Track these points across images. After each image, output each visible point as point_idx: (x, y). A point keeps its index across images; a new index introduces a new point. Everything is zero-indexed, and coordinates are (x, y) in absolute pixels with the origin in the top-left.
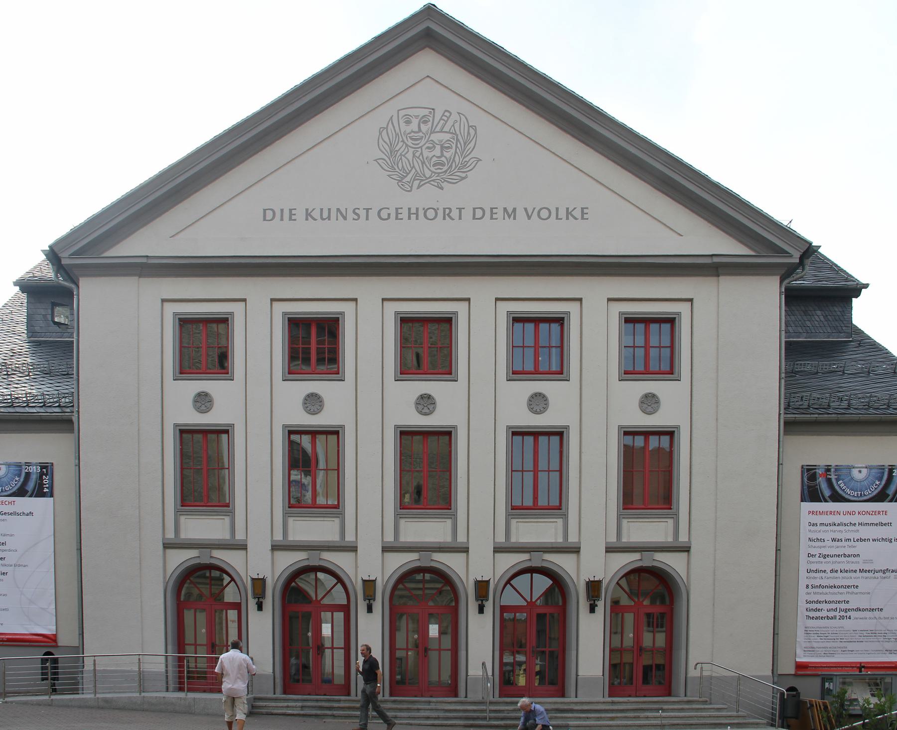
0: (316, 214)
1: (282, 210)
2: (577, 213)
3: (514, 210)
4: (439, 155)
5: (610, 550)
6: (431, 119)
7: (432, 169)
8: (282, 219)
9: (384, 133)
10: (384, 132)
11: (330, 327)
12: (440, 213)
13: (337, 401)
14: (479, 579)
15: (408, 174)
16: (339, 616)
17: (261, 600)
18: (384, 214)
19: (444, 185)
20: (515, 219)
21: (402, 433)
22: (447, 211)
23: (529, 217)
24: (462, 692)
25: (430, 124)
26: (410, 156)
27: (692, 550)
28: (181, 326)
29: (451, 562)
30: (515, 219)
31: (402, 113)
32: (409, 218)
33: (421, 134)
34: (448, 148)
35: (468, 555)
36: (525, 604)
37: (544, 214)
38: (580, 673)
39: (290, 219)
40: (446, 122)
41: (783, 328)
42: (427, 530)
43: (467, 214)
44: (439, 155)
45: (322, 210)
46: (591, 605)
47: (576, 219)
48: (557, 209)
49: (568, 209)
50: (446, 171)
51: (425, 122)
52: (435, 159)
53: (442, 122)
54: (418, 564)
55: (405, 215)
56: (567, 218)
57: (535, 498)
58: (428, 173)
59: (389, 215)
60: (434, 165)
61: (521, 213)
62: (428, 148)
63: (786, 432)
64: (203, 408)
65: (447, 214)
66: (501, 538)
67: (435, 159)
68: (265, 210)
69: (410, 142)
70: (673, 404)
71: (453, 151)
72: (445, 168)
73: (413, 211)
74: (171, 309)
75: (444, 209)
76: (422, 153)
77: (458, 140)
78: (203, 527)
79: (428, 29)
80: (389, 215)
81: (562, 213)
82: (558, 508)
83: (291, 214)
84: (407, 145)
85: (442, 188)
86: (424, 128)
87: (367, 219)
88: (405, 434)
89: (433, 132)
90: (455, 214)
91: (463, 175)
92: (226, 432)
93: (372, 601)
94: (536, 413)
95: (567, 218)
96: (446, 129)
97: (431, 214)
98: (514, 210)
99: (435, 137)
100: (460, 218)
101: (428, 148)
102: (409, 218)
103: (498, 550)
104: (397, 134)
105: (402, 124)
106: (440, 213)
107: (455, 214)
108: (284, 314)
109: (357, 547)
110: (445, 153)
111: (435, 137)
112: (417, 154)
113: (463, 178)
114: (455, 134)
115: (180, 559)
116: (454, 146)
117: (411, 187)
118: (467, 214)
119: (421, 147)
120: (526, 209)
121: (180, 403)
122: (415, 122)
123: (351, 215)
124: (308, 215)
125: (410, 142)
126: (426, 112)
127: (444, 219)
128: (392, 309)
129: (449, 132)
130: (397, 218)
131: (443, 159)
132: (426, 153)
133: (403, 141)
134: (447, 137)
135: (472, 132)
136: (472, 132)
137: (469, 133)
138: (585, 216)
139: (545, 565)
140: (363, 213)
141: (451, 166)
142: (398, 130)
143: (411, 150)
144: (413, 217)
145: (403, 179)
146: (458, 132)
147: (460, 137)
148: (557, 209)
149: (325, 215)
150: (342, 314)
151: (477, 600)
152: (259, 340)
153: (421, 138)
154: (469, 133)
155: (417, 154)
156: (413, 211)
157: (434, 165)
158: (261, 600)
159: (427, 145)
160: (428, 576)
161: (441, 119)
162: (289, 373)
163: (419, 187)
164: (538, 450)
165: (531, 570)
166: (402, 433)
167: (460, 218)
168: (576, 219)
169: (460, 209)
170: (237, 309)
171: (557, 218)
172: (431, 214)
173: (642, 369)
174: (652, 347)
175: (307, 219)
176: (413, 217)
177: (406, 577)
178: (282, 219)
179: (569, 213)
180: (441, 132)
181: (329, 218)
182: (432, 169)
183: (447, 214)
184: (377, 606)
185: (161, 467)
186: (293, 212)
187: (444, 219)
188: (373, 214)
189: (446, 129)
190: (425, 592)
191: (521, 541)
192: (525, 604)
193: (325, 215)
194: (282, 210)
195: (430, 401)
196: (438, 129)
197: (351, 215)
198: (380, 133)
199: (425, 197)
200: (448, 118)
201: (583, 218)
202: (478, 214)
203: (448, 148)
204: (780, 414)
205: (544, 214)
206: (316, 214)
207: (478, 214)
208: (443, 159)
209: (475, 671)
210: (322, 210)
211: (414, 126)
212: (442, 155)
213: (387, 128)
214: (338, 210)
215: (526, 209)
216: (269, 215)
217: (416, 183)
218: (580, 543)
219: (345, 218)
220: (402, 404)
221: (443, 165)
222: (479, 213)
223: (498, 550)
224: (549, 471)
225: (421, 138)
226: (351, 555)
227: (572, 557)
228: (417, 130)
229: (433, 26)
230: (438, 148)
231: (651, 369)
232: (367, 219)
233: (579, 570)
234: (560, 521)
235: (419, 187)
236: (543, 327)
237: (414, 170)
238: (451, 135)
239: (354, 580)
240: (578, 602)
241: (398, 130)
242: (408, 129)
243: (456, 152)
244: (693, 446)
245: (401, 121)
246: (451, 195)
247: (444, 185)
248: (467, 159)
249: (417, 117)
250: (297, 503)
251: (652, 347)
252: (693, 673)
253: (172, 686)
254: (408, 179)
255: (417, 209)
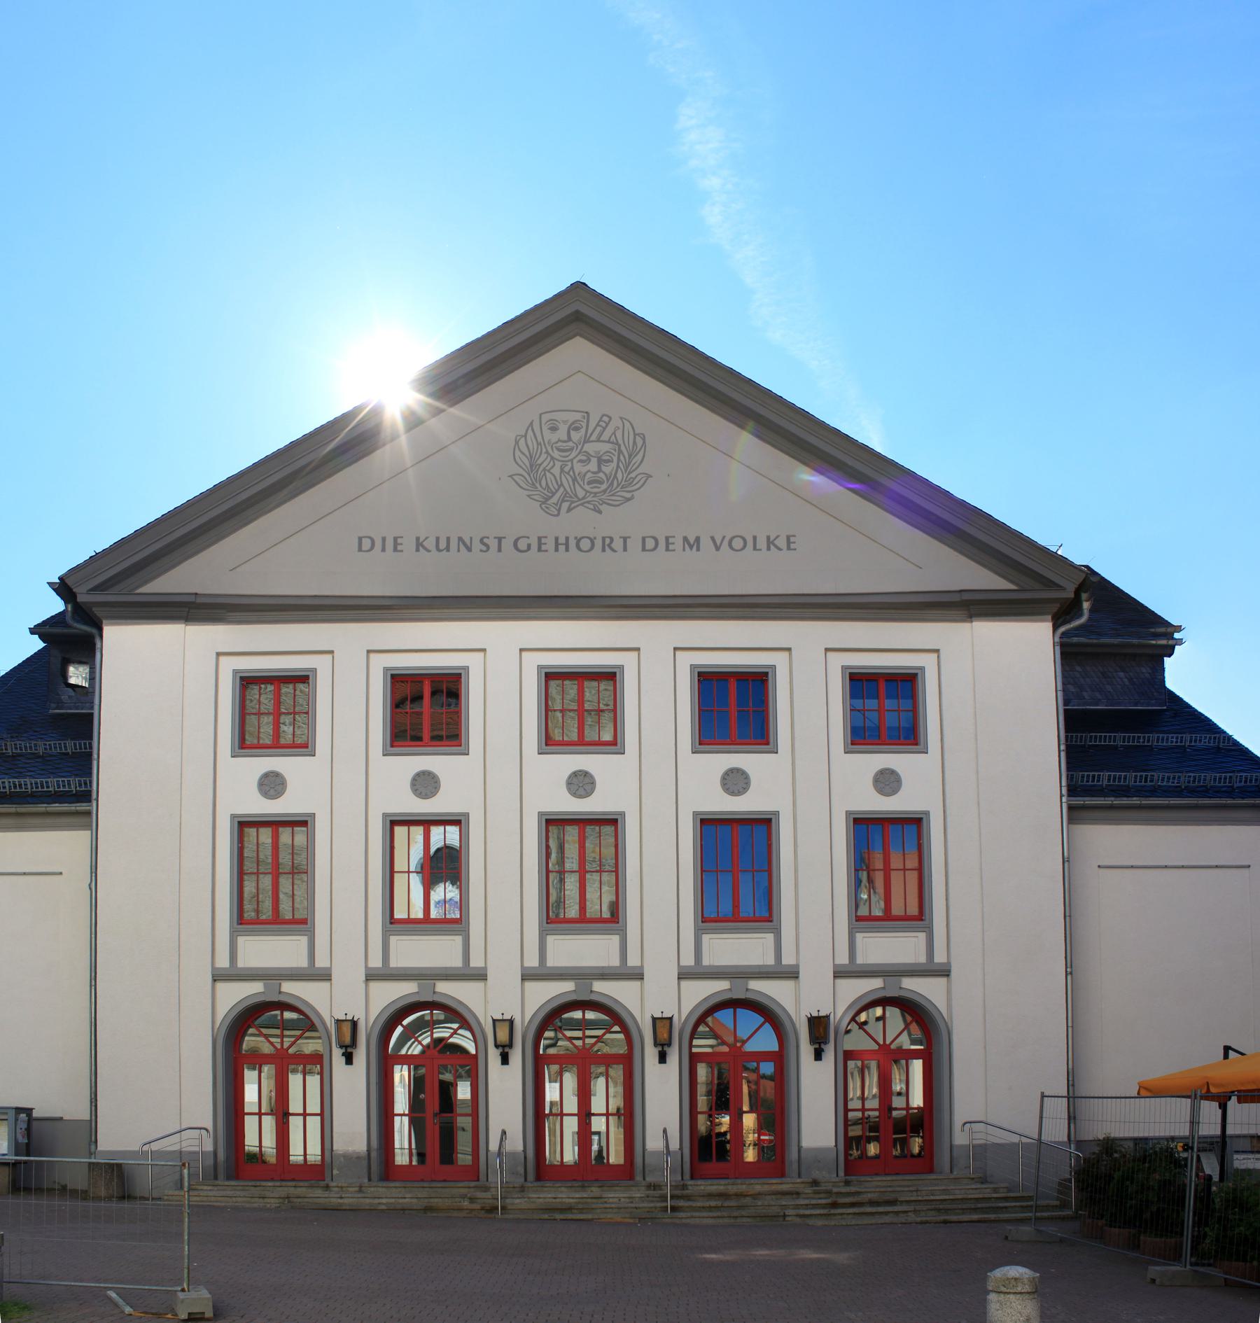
0: (430, 544)
1: (384, 539)
2: (782, 542)
3: (698, 540)
4: (595, 469)
5: (528, 976)
6: (584, 425)
7: (587, 487)
8: (383, 550)
9: (522, 442)
10: (522, 442)
11: (754, 686)
12: (598, 543)
13: (769, 781)
14: (815, 1014)
15: (554, 494)
16: (617, 1072)
17: (666, 1048)
18: (522, 545)
19: (603, 507)
20: (698, 550)
21: (703, 822)
22: (608, 541)
23: (718, 548)
24: (482, 1177)
25: (583, 431)
26: (556, 471)
27: (953, 974)
28: (393, 684)
29: (775, 991)
30: (698, 550)
31: (545, 418)
32: (557, 550)
33: (570, 444)
34: (608, 461)
35: (949, 982)
36: (877, 1047)
37: (738, 543)
38: (335, 1148)
39: (395, 550)
40: (604, 429)
41: (1060, 687)
42: (739, 949)
43: (634, 545)
44: (595, 469)
45: (438, 539)
46: (816, 1050)
47: (780, 549)
48: (755, 538)
49: (768, 538)
50: (605, 491)
51: (577, 429)
52: (589, 475)
53: (599, 429)
54: (573, 997)
55: (550, 545)
56: (769, 549)
57: (736, 906)
58: (581, 493)
59: (529, 546)
60: (589, 483)
61: (706, 543)
62: (581, 461)
63: (1071, 820)
64: (581, 791)
65: (607, 544)
66: (843, 959)
67: (589, 475)
68: (360, 539)
69: (556, 454)
70: (919, 782)
71: (614, 465)
72: (604, 487)
73: (562, 540)
74: (229, 666)
75: (604, 539)
76: (572, 468)
77: (620, 452)
78: (269, 951)
79: (577, 312)
80: (529, 546)
81: (762, 543)
82: (919, 918)
83: (668, 543)
84: (552, 458)
85: (600, 512)
86: (576, 436)
87: (500, 550)
88: (708, 824)
89: (587, 441)
90: (618, 544)
91: (628, 495)
92: (304, 823)
93: (666, 1048)
94: (733, 793)
95: (769, 549)
96: (605, 437)
97: (585, 544)
98: (698, 540)
99: (591, 448)
100: (625, 549)
101: (581, 461)
102: (557, 550)
103: (839, 973)
104: (539, 444)
105: (547, 433)
106: (598, 543)
107: (618, 544)
108: (693, 667)
109: (330, 975)
110: (603, 468)
111: (591, 448)
112: (567, 469)
113: (628, 500)
114: (617, 444)
115: (235, 995)
116: (615, 459)
117: (559, 510)
118: (634, 545)
119: (572, 460)
120: (713, 539)
121: (240, 786)
122: (563, 429)
123: (477, 546)
124: (419, 545)
125: (556, 454)
126: (578, 416)
127: (604, 550)
128: (838, 662)
129: (609, 442)
130: (540, 550)
131: (601, 475)
132: (579, 468)
133: (547, 452)
134: (608, 447)
135: (639, 441)
136: (639, 441)
137: (635, 442)
138: (792, 546)
139: (750, 996)
140: (493, 544)
141: (612, 484)
142: (540, 439)
143: (558, 464)
144: (562, 548)
145: (547, 500)
146: (620, 442)
147: (623, 448)
148: (755, 538)
149: (443, 545)
150: (922, 669)
151: (656, 1044)
152: (810, 700)
153: (571, 449)
154: (635, 442)
155: (567, 469)
156: (562, 540)
157: (589, 483)
158: (507, 1050)
159: (580, 457)
160: (590, 1015)
161: (598, 425)
162: (700, 744)
163: (569, 510)
164: (580, 848)
165: (884, 1002)
166: (703, 822)
167: (625, 549)
168: (780, 549)
169: (625, 539)
170: (320, 664)
171: (755, 548)
172: (585, 544)
173: (575, 737)
174: (885, 708)
175: (417, 550)
176: (562, 548)
177: (553, 1017)
178: (383, 550)
179: (770, 543)
180: (598, 440)
181: (448, 549)
182: (587, 487)
183: (607, 544)
184: (516, 1056)
185: (208, 871)
186: (671, 540)
187: (604, 550)
188: (507, 545)
189: (605, 437)
190: (579, 1031)
191: (717, 964)
192: (877, 1047)
193: (443, 545)
194: (384, 539)
195: (587, 780)
196: (594, 438)
197: (477, 546)
198: (517, 442)
199: (578, 522)
200: (607, 424)
201: (789, 548)
202: (649, 544)
203: (608, 461)
204: (1061, 796)
205: (738, 543)
206: (430, 544)
207: (649, 544)
208: (601, 475)
209: (654, 1143)
210: (438, 539)
211: (562, 433)
212: (600, 470)
213: (525, 436)
214: (460, 539)
215: (713, 539)
216: (366, 544)
217: (565, 505)
218: (642, 967)
219: (469, 549)
220: (703, 781)
221: (601, 483)
222: (650, 544)
223: (839, 973)
224: (904, 870)
225: (571, 449)
226: (635, 984)
227: (788, 985)
228: (565, 438)
229: (585, 310)
230: (594, 461)
231: (282, 741)
232: (500, 550)
233: (799, 1001)
234: (770, 937)
235: (569, 510)
236: (590, 686)
237: (562, 490)
238: (610, 446)
239: (483, 1022)
240: (798, 1047)
241: (540, 439)
242: (554, 437)
243: (618, 466)
244: (949, 837)
245: (545, 428)
246: (613, 521)
247: (603, 507)
248: (633, 475)
249: (565, 422)
250: (713, 917)
251: (885, 708)
252: (960, 1139)
253: (375, 1175)
254: (554, 500)
255: (567, 539)
